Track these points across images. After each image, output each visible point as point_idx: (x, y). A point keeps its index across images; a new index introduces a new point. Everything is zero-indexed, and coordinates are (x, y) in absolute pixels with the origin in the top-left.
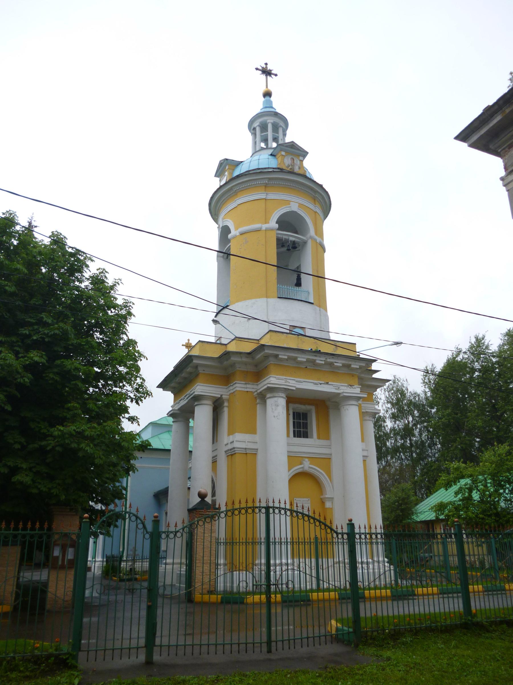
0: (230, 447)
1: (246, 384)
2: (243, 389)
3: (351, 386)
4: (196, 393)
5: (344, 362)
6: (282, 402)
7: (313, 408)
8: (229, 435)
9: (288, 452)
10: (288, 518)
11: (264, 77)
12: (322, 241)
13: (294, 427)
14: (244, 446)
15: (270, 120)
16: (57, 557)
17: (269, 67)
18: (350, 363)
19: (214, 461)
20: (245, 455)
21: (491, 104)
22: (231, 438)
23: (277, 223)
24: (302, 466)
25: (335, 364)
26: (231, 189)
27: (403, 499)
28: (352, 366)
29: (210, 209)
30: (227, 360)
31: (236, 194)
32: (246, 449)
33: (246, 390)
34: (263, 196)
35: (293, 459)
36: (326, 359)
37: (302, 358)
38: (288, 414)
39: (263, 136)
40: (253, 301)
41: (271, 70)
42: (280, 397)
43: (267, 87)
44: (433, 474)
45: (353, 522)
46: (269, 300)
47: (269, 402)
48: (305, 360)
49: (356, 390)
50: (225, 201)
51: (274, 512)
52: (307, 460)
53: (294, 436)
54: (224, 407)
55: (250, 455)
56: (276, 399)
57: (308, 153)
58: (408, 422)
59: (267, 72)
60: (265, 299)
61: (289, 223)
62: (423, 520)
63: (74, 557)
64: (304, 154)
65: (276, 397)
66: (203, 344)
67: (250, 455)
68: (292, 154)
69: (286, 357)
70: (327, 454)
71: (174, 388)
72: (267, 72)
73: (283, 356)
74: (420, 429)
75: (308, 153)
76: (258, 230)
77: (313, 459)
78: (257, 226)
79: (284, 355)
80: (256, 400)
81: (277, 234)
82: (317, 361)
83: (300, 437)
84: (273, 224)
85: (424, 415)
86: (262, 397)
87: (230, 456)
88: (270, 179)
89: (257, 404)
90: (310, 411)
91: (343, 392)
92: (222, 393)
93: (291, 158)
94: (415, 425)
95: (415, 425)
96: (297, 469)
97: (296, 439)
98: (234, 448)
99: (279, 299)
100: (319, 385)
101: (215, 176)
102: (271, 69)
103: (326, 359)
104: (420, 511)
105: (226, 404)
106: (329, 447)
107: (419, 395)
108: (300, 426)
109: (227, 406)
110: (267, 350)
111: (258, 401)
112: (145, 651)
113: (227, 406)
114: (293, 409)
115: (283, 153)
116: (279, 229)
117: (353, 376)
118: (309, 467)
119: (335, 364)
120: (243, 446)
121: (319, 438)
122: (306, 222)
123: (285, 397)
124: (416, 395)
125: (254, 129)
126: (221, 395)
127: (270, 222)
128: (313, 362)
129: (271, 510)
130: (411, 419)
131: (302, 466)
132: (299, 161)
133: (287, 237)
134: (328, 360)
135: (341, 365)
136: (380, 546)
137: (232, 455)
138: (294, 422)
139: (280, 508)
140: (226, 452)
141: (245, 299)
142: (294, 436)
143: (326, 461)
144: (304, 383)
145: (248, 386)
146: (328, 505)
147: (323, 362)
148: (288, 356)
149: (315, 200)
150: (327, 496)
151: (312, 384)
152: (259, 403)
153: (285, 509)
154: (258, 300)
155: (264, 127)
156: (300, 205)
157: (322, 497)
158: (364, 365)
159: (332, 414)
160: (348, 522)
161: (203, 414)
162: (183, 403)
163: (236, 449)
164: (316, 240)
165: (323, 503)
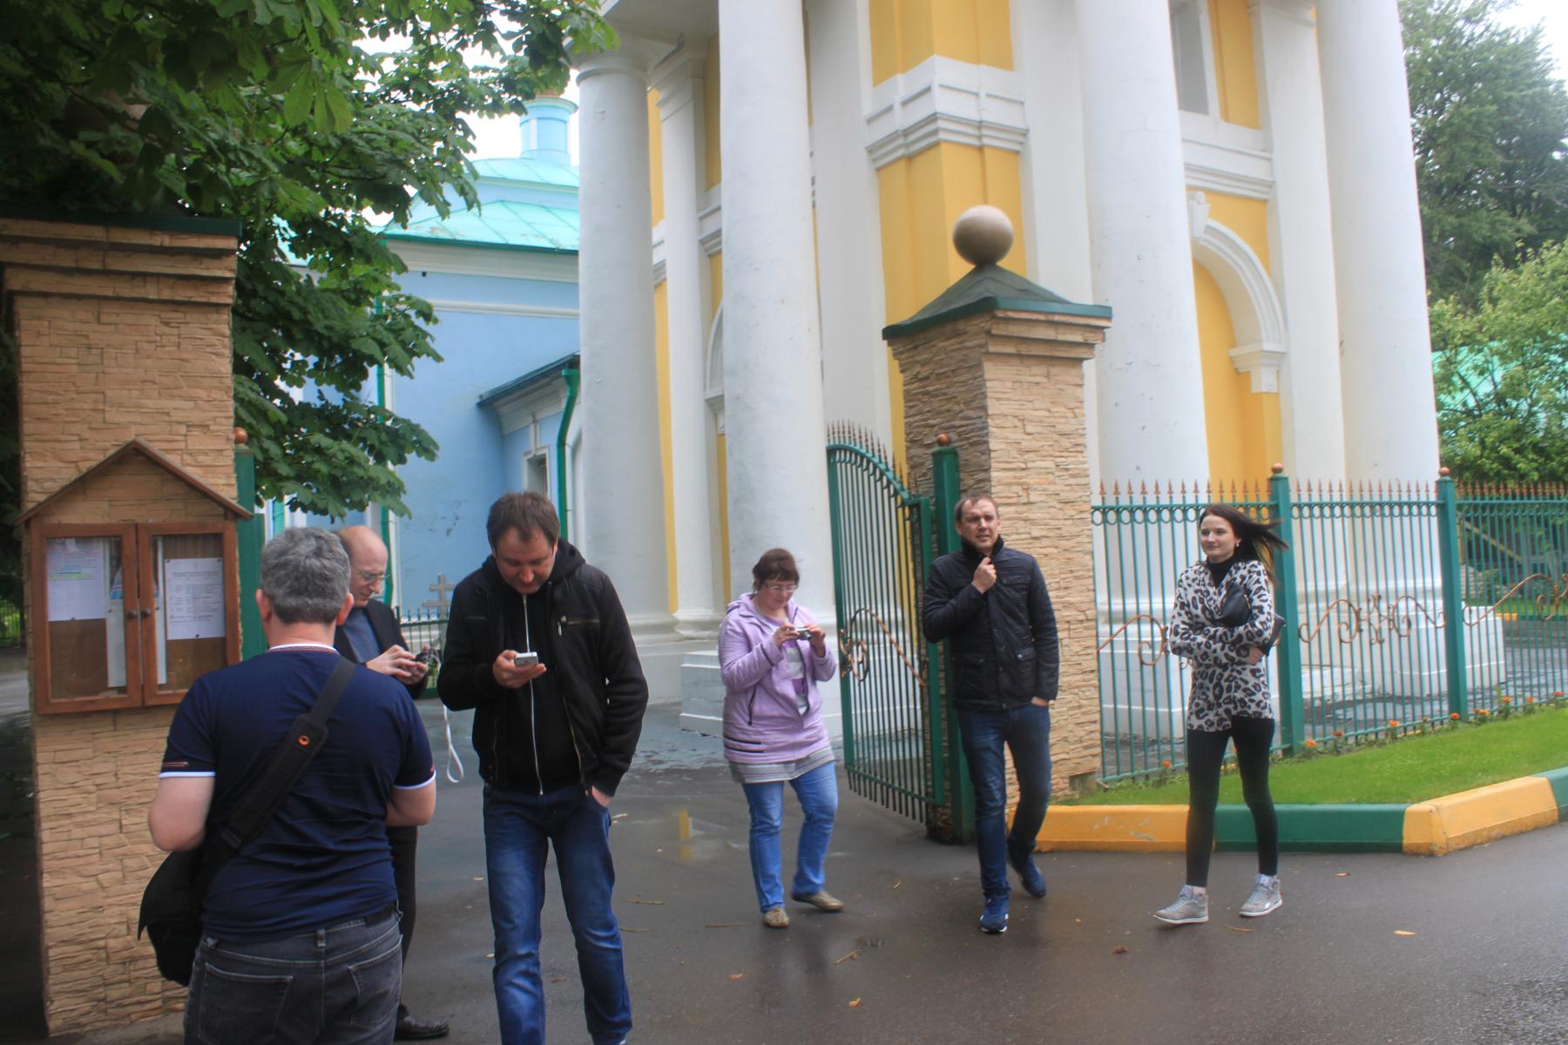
16: (93, 631)
22: (902, 85)
32: (980, 125)
45: (1284, 474)
63: (229, 618)
70: (1229, 176)
87: (902, 164)
98: (933, 118)
112: (70, 319)
118: (1209, 229)
120: (965, 108)
137: (910, 158)
140: (871, 150)
146: (1264, 381)
157: (1234, 352)
160: (1270, 474)
163: (941, 124)
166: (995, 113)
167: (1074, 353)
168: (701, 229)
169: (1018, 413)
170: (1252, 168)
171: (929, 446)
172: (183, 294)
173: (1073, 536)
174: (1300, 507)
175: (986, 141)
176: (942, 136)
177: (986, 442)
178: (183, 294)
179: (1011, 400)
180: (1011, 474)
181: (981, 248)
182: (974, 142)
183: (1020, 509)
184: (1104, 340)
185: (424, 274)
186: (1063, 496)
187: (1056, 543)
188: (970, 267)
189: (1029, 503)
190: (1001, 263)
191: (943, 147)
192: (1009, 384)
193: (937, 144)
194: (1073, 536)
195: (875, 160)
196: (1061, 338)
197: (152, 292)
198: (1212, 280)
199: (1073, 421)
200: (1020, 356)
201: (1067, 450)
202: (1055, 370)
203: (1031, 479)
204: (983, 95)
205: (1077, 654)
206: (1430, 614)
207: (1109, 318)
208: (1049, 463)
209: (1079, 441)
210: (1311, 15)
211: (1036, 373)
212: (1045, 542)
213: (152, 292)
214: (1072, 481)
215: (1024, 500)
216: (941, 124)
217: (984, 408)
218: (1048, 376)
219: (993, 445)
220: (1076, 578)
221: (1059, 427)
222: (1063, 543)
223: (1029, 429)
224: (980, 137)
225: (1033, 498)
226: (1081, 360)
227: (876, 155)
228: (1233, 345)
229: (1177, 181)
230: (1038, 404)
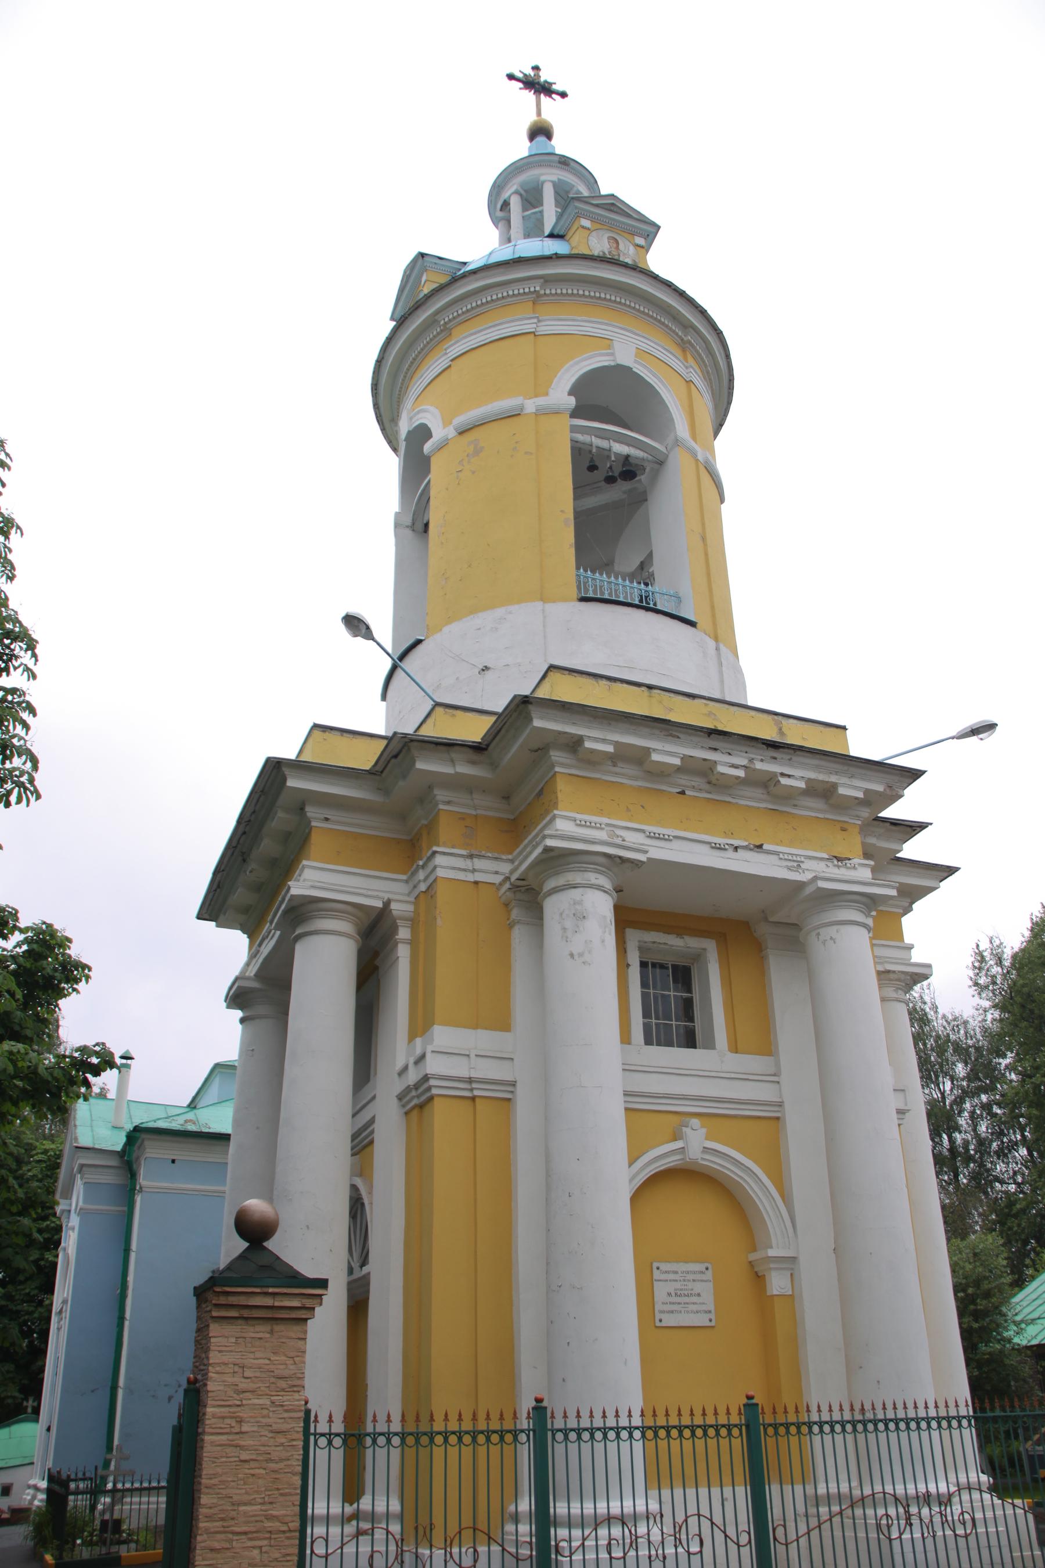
0: (413, 1076)
1: (471, 856)
2: (461, 876)
3: (839, 859)
5: (812, 775)
6: (599, 906)
7: (710, 948)
8: (411, 1038)
9: (626, 1094)
11: (529, 96)
12: (710, 458)
13: (646, 1014)
15: (549, 177)
17: (544, 76)
18: (833, 779)
19: (362, 1143)
20: (469, 1102)
23: (571, 393)
24: (679, 1144)
25: (784, 781)
26: (432, 321)
27: (977, 1283)
28: (841, 791)
29: (376, 406)
30: (404, 777)
31: (447, 332)
32: (470, 1080)
33: (471, 878)
34: (528, 326)
35: (643, 1116)
36: (751, 760)
37: (667, 753)
38: (623, 965)
39: (529, 216)
40: (500, 612)
41: (551, 84)
42: (591, 886)
43: (539, 113)
44: (1019, 1225)
45: (545, 1404)
46: (549, 607)
47: (554, 907)
48: (677, 761)
49: (859, 874)
50: (412, 369)
52: (695, 1122)
53: (648, 1042)
55: (492, 1103)
56: (575, 894)
57: (659, 227)
58: (943, 1094)
59: (536, 85)
60: (539, 605)
61: (612, 396)
62: (1034, 1342)
64: (649, 230)
65: (575, 887)
66: (327, 735)
67: (492, 1103)
68: (611, 226)
69: (610, 749)
71: (246, 910)
72: (536, 85)
73: (599, 740)
74: (972, 1113)
75: (659, 227)
76: (514, 415)
77: (719, 1118)
79: (604, 741)
80: (509, 912)
81: (574, 429)
82: (721, 769)
83: (670, 1044)
85: (983, 1074)
86: (528, 897)
87: (415, 1112)
88: (547, 280)
89: (511, 926)
90: (699, 957)
91: (815, 878)
92: (386, 896)
93: (609, 238)
94: (959, 1101)
95: (959, 1101)
96: (661, 1155)
97: (654, 1049)
98: (426, 1078)
99: (583, 604)
100: (730, 853)
102: (549, 80)
103: (751, 760)
104: (1018, 1318)
105: (403, 933)
106: (774, 1077)
107: (966, 1023)
108: (670, 1007)
109: (404, 941)
110: (542, 718)
111: (515, 913)
113: (404, 941)
114: (641, 949)
115: (586, 223)
116: (575, 414)
117: (844, 830)
118: (706, 1150)
119: (784, 781)
120: (460, 1069)
121: (734, 1048)
122: (662, 402)
123: (608, 885)
124: (958, 1023)
125: (506, 205)
126: (387, 904)
127: (551, 391)
128: (705, 771)
130: (948, 1085)
131: (679, 1144)
132: (632, 248)
133: (604, 444)
134: (759, 765)
135: (802, 785)
136: (966, 1433)
137: (421, 1107)
138: (645, 997)
140: (400, 1098)
141: (474, 611)
142: (648, 1042)
143: (765, 1128)
144: (676, 844)
145: (478, 863)
146: (778, 1283)
147: (741, 773)
148: (617, 744)
149: (684, 350)
150: (771, 1253)
151: (706, 849)
154: (514, 608)
155: (532, 198)
156: (640, 352)
157: (752, 1257)
158: (880, 788)
159: (780, 974)
161: (324, 968)
162: (267, 948)
163: (432, 1082)
164: (694, 455)
165: (758, 1279)
169: (238, 1361)
173: (281, 1460)
174: (566, 1431)
175: (476, 1093)
176: (434, 1091)
180: (227, 1409)
181: (254, 1232)
183: (231, 1437)
184: (321, 1304)
185: (173, 1161)
186: (275, 1427)
187: (264, 1465)
188: (246, 1244)
189: (241, 1433)
190: (265, 1244)
191: (436, 1100)
192: (233, 1340)
193: (431, 1098)
194: (281, 1460)
195: (404, 1106)
196: (277, 1304)
199: (292, 1367)
200: (246, 1319)
201: (283, 1390)
202: (277, 1328)
203: (243, 1414)
204: (472, 1056)
205: (276, 1560)
206: (731, 1531)
208: (265, 1401)
209: (298, 1382)
211: (261, 1331)
212: (252, 1464)
214: (286, 1415)
215: (237, 1430)
216: (432, 1082)
218: (272, 1332)
220: (281, 1495)
221: (277, 1372)
222: (272, 1465)
223: (246, 1374)
224: (472, 1090)
225: (245, 1428)
226: (306, 1320)
227: (405, 1100)
228: (754, 1249)
230: (258, 1355)
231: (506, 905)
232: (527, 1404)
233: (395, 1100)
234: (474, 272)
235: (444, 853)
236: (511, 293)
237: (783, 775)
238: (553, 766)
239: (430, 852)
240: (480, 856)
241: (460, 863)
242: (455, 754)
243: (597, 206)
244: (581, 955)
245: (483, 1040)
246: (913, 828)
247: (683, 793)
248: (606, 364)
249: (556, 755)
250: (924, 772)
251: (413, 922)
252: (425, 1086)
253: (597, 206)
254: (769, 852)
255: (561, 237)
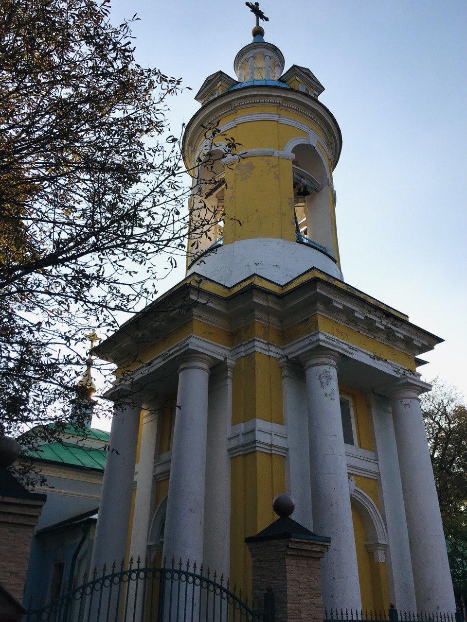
2: (264, 352)
4: (190, 347)
10: (197, 588)
14: (269, 441)
18: (413, 337)
21: (338, 209)
26: (229, 104)
31: (235, 110)
32: (271, 446)
33: (267, 353)
34: (276, 118)
51: (187, 580)
54: (226, 378)
64: (321, 89)
78: (269, 150)
79: (340, 303)
84: (288, 151)
88: (285, 98)
101: (196, 98)
105: (229, 374)
115: (298, 79)
126: (225, 359)
129: (168, 575)
139: (187, 574)
140: (229, 450)
146: (381, 556)
148: (344, 306)
152: (286, 376)
153: (193, 575)
163: (257, 444)
166: (278, 441)
167: (317, 555)
168: (154, 471)
170: (371, 467)
171: (262, 590)
172: (20, 520)
175: (273, 452)
176: (258, 449)
177: (286, 591)
178: (20, 520)
179: (295, 575)
180: (294, 605)
182: (270, 452)
193: (256, 451)
197: (10, 519)
198: (356, 506)
207: (330, 542)
208: (308, 601)
210: (390, 409)
213: (10, 519)
216: (257, 444)
217: (285, 577)
219: (288, 593)
223: (301, 586)
224: (271, 450)
226: (319, 558)
229: (345, 471)
231: (281, 368)
232: (387, 608)
233: (226, 451)
234: (244, 88)
235: (258, 341)
236: (261, 101)
237: (397, 332)
238: (193, 316)
239: (253, 338)
240: (271, 345)
241: (263, 346)
242: (270, 298)
243: (303, 72)
244: (330, 395)
245: (275, 427)
246: (424, 363)
247: (359, 332)
248: (303, 143)
249: (320, 306)
250: (443, 340)
251: (235, 369)
252: (253, 445)
253: (303, 72)
254: (389, 363)
255: (284, 82)
